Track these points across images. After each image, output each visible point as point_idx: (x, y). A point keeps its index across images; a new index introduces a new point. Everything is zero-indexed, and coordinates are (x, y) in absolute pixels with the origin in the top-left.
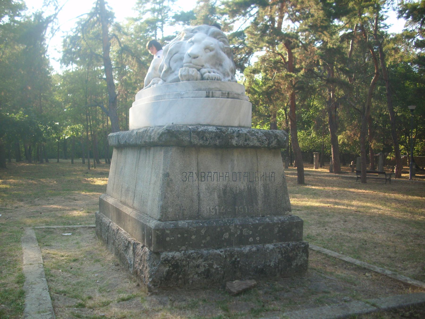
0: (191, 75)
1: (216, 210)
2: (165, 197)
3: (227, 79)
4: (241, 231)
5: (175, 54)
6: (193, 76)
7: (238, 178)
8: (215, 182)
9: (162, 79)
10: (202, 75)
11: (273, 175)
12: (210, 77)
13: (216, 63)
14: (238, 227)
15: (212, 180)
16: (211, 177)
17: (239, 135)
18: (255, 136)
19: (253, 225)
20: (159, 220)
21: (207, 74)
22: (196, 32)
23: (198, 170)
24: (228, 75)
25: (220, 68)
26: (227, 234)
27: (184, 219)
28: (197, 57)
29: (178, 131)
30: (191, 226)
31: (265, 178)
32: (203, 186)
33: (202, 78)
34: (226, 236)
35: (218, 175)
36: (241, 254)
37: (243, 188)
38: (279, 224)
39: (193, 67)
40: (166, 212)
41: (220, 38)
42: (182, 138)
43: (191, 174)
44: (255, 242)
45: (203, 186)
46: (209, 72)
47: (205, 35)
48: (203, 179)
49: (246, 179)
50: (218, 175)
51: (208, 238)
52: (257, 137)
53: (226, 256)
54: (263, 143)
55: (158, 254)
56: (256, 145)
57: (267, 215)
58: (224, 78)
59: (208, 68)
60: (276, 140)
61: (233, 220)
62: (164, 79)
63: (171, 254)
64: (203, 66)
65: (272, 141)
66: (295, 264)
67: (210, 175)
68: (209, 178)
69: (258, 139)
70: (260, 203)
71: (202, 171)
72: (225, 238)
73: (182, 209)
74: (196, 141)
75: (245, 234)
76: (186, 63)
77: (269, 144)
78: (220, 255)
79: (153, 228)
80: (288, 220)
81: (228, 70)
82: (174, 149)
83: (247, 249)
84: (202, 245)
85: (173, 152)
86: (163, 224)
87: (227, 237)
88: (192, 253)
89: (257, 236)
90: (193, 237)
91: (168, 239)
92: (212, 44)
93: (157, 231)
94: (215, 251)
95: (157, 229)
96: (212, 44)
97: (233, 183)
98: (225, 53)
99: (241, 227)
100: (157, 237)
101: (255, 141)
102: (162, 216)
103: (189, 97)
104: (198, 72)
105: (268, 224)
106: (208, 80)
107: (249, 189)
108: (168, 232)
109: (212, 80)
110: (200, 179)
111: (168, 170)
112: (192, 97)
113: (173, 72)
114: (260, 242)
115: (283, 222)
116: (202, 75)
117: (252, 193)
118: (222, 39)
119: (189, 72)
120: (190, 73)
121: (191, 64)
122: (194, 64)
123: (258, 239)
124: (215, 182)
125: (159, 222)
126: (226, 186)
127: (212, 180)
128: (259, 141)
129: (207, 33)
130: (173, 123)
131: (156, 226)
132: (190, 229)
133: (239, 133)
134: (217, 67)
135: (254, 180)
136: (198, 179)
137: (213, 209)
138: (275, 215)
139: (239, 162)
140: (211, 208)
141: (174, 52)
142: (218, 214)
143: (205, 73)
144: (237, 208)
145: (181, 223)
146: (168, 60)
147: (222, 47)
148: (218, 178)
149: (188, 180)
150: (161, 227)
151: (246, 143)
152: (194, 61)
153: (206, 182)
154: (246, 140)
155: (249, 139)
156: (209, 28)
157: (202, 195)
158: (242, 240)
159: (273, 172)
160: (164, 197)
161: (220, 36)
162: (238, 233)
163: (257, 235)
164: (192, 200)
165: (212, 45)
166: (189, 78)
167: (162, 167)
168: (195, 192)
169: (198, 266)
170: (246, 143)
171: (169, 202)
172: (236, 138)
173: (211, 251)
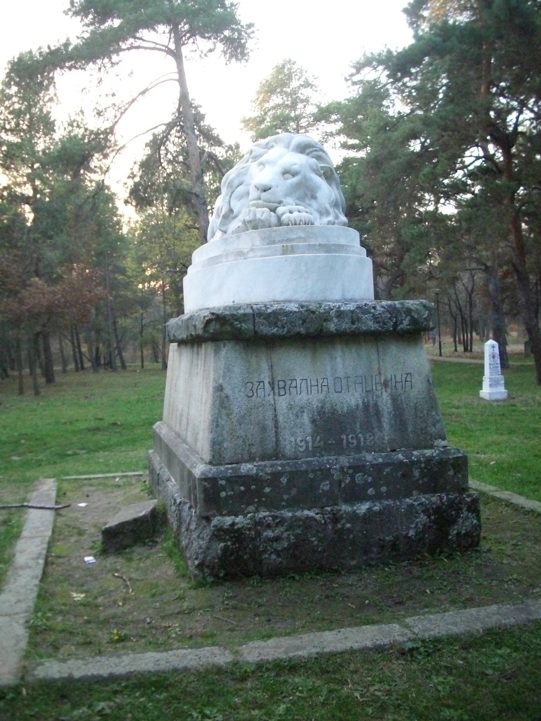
0: (260, 219)
1: (307, 443)
2: (217, 426)
3: (326, 220)
4: (352, 477)
5: (238, 186)
6: (262, 221)
7: (345, 387)
8: (304, 394)
9: (220, 230)
10: (279, 218)
11: (408, 379)
12: (292, 219)
13: (306, 195)
14: (345, 470)
15: (299, 393)
16: (296, 387)
17: (340, 314)
18: (370, 313)
19: (373, 466)
20: (210, 463)
21: (288, 215)
22: (272, 147)
23: (272, 376)
24: (328, 213)
25: (314, 203)
26: (328, 482)
27: (251, 459)
28: (270, 189)
29: (233, 315)
30: (262, 471)
31: (394, 384)
32: (282, 403)
33: (280, 223)
34: (325, 486)
35: (309, 385)
36: (354, 517)
37: (353, 402)
38: (421, 463)
39: (263, 207)
40: (220, 449)
41: (311, 152)
42: (239, 326)
43: (262, 384)
44: (378, 497)
45: (282, 403)
46: (291, 212)
47: (286, 150)
48: (282, 392)
49: (359, 389)
50: (309, 385)
51: (294, 491)
52: (374, 316)
53: (325, 521)
54: (384, 323)
55: (208, 519)
56: (373, 329)
57: (400, 448)
58: (320, 218)
59: (289, 204)
60: (409, 318)
61: (336, 459)
62: (223, 229)
63: (228, 520)
64: (280, 203)
65: (402, 320)
66: (455, 532)
67: (294, 384)
68: (293, 390)
69: (376, 318)
70: (386, 425)
71: (279, 378)
72: (322, 490)
73: (247, 444)
74: (266, 330)
75: (360, 482)
76: (254, 200)
77: (395, 325)
78: (316, 520)
79: (197, 477)
80: (438, 455)
81: (328, 206)
82: (229, 345)
83: (363, 508)
84: (283, 503)
85: (228, 352)
86: (214, 469)
87: (327, 488)
88: (264, 517)
89: (381, 486)
90: (267, 490)
91: (223, 494)
92: (295, 164)
93: (203, 482)
94: (306, 512)
95: (205, 479)
96: (295, 164)
97: (336, 395)
98: (320, 176)
99: (351, 471)
100: (205, 491)
101: (371, 323)
102: (213, 456)
103: (256, 256)
104: (272, 213)
105: (401, 463)
106: (288, 225)
107: (366, 406)
108: (223, 482)
109: (296, 224)
110: (277, 391)
111: (221, 381)
112: (261, 256)
113: (236, 217)
114: (389, 496)
115: (429, 460)
116: (279, 218)
117: (370, 412)
118: (316, 153)
119: (255, 215)
120: (258, 216)
121: (260, 202)
122: (264, 201)
123: (384, 489)
124: (304, 394)
125: (209, 467)
126: (323, 402)
127: (299, 393)
128: (378, 322)
129: (288, 147)
130: (234, 302)
131: (203, 474)
132: (261, 476)
133: (340, 311)
134: (307, 201)
135: (374, 388)
136: (274, 393)
137: (301, 441)
138: (416, 448)
139: (343, 362)
140: (299, 439)
141: (236, 182)
142: (310, 449)
143: (283, 214)
144: (345, 437)
145: (246, 468)
146: (228, 198)
147: (315, 167)
148: (309, 389)
149: (255, 394)
150: (210, 475)
151: (355, 326)
152: (264, 195)
153: (287, 396)
154: (353, 323)
155: (359, 319)
156: (292, 139)
157: (281, 418)
158: (355, 495)
159: (407, 374)
160: (215, 425)
161: (311, 149)
162: (347, 481)
163: (382, 482)
164: (264, 429)
165: (294, 167)
166: (254, 225)
167: (212, 376)
168: (270, 414)
169: (277, 539)
170: (355, 326)
171: (224, 432)
172: (335, 320)
173: (298, 514)
